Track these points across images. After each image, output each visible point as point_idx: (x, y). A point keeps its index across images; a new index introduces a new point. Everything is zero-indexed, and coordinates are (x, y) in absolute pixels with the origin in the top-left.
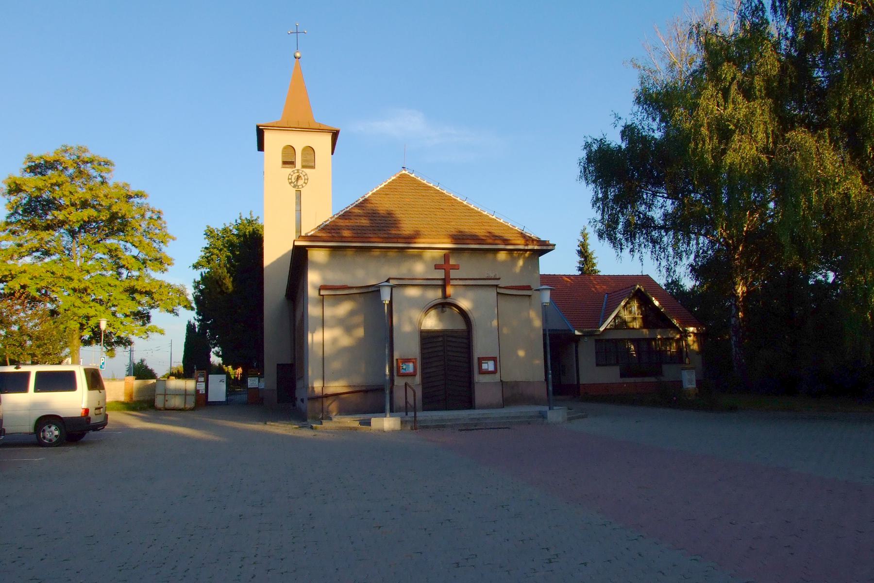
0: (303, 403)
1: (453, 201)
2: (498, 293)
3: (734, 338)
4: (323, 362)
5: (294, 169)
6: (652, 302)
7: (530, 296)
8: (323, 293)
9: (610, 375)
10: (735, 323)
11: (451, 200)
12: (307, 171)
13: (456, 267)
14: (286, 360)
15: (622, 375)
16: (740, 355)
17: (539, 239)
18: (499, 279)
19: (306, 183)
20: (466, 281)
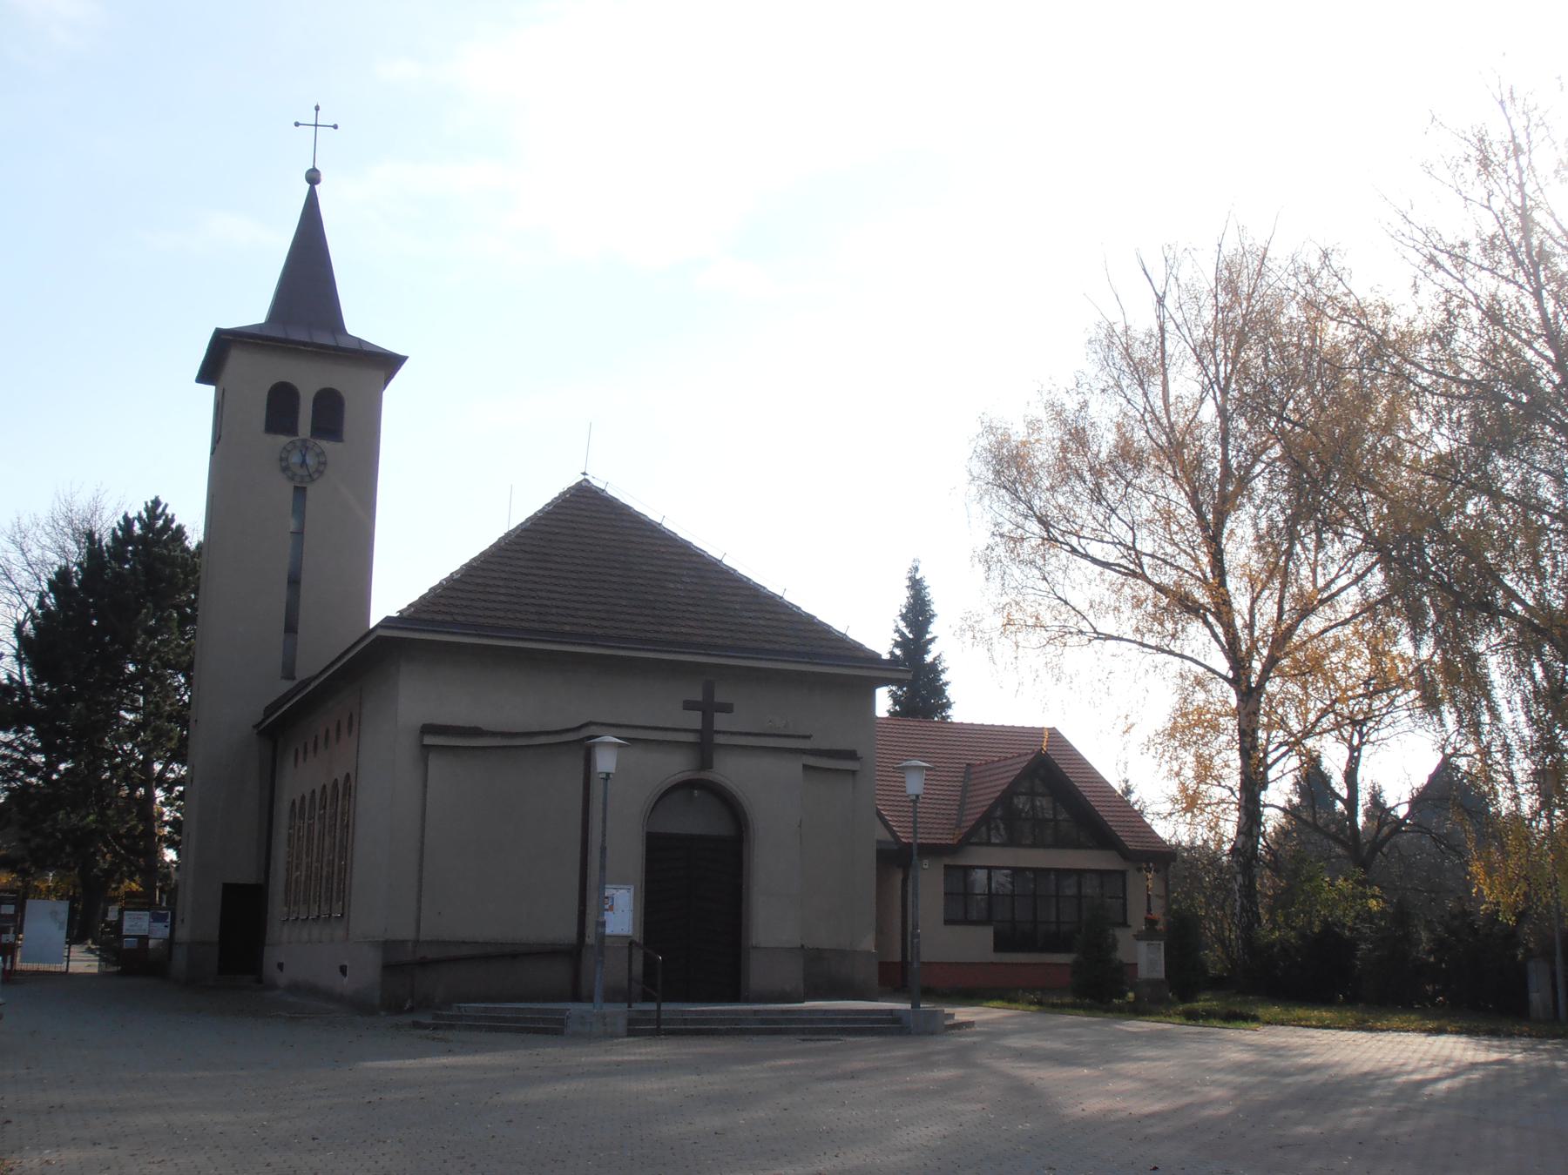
0: (282, 970)
1: (694, 559)
2: (805, 767)
3: (1240, 878)
4: (421, 870)
5: (294, 438)
6: (117, 763)
7: (854, 773)
8: (429, 740)
9: (975, 944)
10: (1243, 847)
11: (691, 555)
12: (325, 445)
13: (727, 708)
14: (246, 874)
15: (1001, 944)
16: (1250, 914)
17: (1447, 1061)
18: (808, 737)
19: (281, 459)
20: (750, 738)
